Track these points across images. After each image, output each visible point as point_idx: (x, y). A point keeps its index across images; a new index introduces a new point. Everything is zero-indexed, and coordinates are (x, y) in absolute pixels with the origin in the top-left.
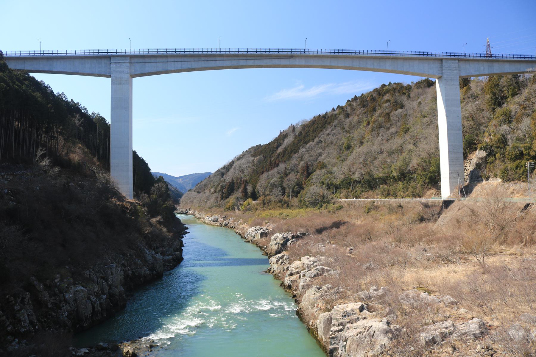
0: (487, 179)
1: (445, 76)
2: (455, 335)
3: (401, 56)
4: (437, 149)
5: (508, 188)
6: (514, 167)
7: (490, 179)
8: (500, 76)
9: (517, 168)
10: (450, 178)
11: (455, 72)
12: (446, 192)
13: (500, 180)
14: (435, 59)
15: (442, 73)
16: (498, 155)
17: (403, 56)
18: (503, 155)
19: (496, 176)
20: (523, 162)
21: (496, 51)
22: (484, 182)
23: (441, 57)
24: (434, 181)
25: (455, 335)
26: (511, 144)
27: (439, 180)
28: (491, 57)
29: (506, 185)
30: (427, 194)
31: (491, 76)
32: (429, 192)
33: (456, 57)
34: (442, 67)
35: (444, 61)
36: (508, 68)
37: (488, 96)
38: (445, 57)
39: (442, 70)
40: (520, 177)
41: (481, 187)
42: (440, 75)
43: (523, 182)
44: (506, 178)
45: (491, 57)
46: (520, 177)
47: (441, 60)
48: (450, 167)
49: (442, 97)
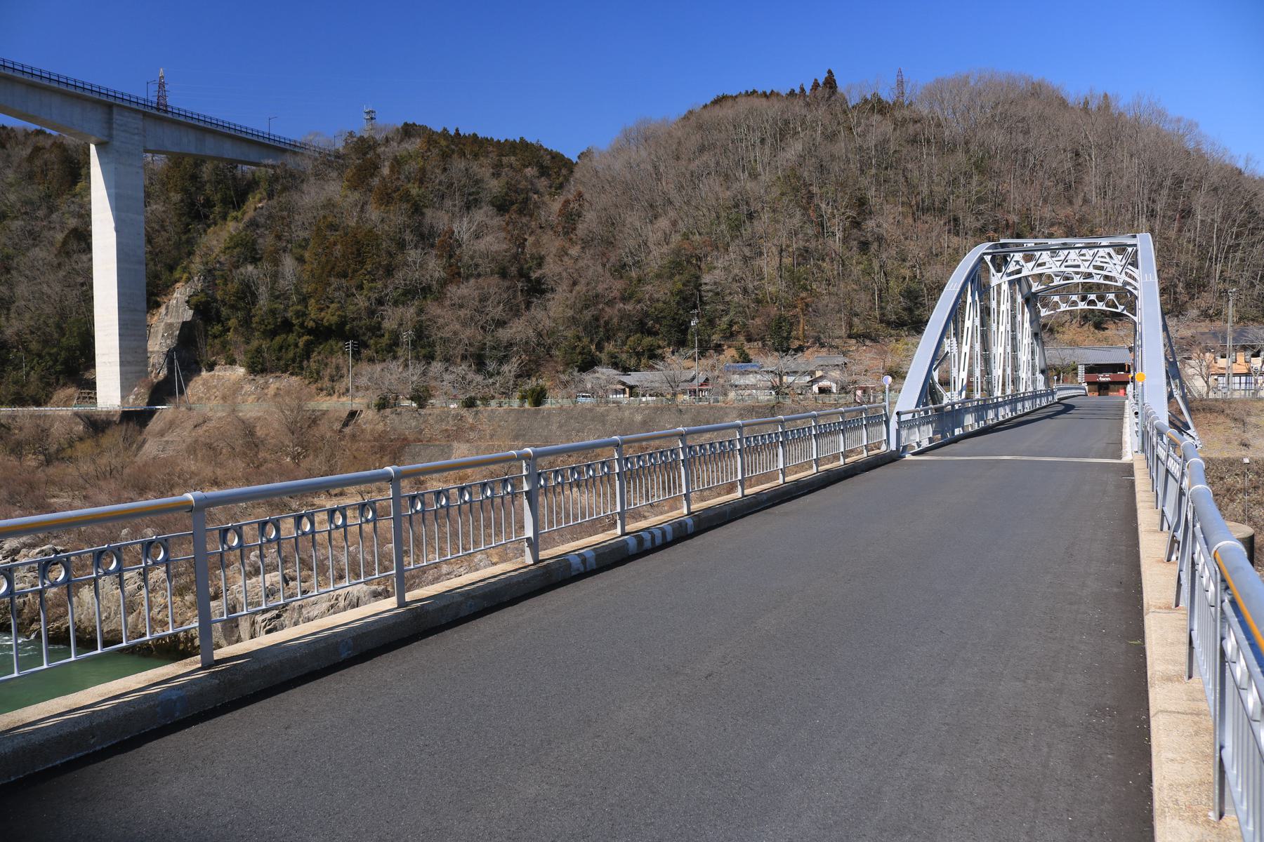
0: (211, 367)
1: (116, 143)
2: (872, 192)
3: (25, 77)
4: (88, 299)
5: (266, 386)
6: (276, 347)
7: (217, 368)
8: (199, 161)
9: (280, 349)
10: (122, 364)
11: (136, 137)
12: (109, 392)
13: (241, 371)
14: (98, 102)
15: (110, 136)
16: (232, 323)
17: (55, 85)
18: (246, 322)
19: (232, 362)
20: (291, 338)
21: (178, 100)
22: (204, 373)
23: (111, 100)
24: (77, 365)
25: (872, 192)
26: (263, 301)
27: (90, 362)
28: (166, 111)
29: (260, 380)
30: (55, 398)
31: (177, 159)
32: (61, 394)
33: (141, 108)
34: (109, 122)
35: (115, 110)
36: (230, 150)
37: (176, 197)
38: (118, 102)
39: (110, 128)
40: (287, 366)
41: (203, 384)
42: (105, 139)
43: (292, 374)
44: (257, 367)
45: (166, 111)
46: (287, 366)
47: (110, 106)
48: (120, 340)
49: (107, 188)
